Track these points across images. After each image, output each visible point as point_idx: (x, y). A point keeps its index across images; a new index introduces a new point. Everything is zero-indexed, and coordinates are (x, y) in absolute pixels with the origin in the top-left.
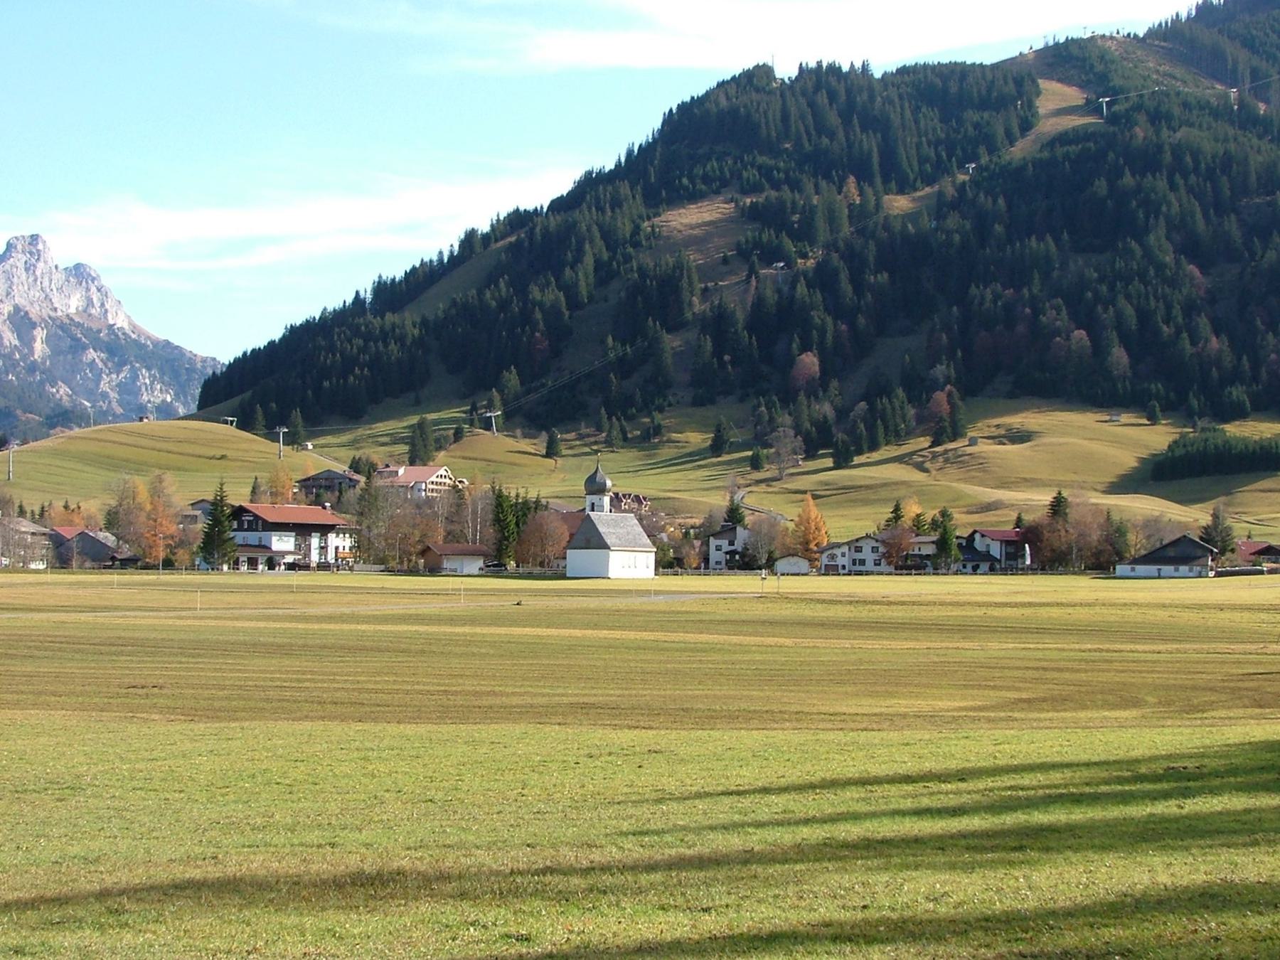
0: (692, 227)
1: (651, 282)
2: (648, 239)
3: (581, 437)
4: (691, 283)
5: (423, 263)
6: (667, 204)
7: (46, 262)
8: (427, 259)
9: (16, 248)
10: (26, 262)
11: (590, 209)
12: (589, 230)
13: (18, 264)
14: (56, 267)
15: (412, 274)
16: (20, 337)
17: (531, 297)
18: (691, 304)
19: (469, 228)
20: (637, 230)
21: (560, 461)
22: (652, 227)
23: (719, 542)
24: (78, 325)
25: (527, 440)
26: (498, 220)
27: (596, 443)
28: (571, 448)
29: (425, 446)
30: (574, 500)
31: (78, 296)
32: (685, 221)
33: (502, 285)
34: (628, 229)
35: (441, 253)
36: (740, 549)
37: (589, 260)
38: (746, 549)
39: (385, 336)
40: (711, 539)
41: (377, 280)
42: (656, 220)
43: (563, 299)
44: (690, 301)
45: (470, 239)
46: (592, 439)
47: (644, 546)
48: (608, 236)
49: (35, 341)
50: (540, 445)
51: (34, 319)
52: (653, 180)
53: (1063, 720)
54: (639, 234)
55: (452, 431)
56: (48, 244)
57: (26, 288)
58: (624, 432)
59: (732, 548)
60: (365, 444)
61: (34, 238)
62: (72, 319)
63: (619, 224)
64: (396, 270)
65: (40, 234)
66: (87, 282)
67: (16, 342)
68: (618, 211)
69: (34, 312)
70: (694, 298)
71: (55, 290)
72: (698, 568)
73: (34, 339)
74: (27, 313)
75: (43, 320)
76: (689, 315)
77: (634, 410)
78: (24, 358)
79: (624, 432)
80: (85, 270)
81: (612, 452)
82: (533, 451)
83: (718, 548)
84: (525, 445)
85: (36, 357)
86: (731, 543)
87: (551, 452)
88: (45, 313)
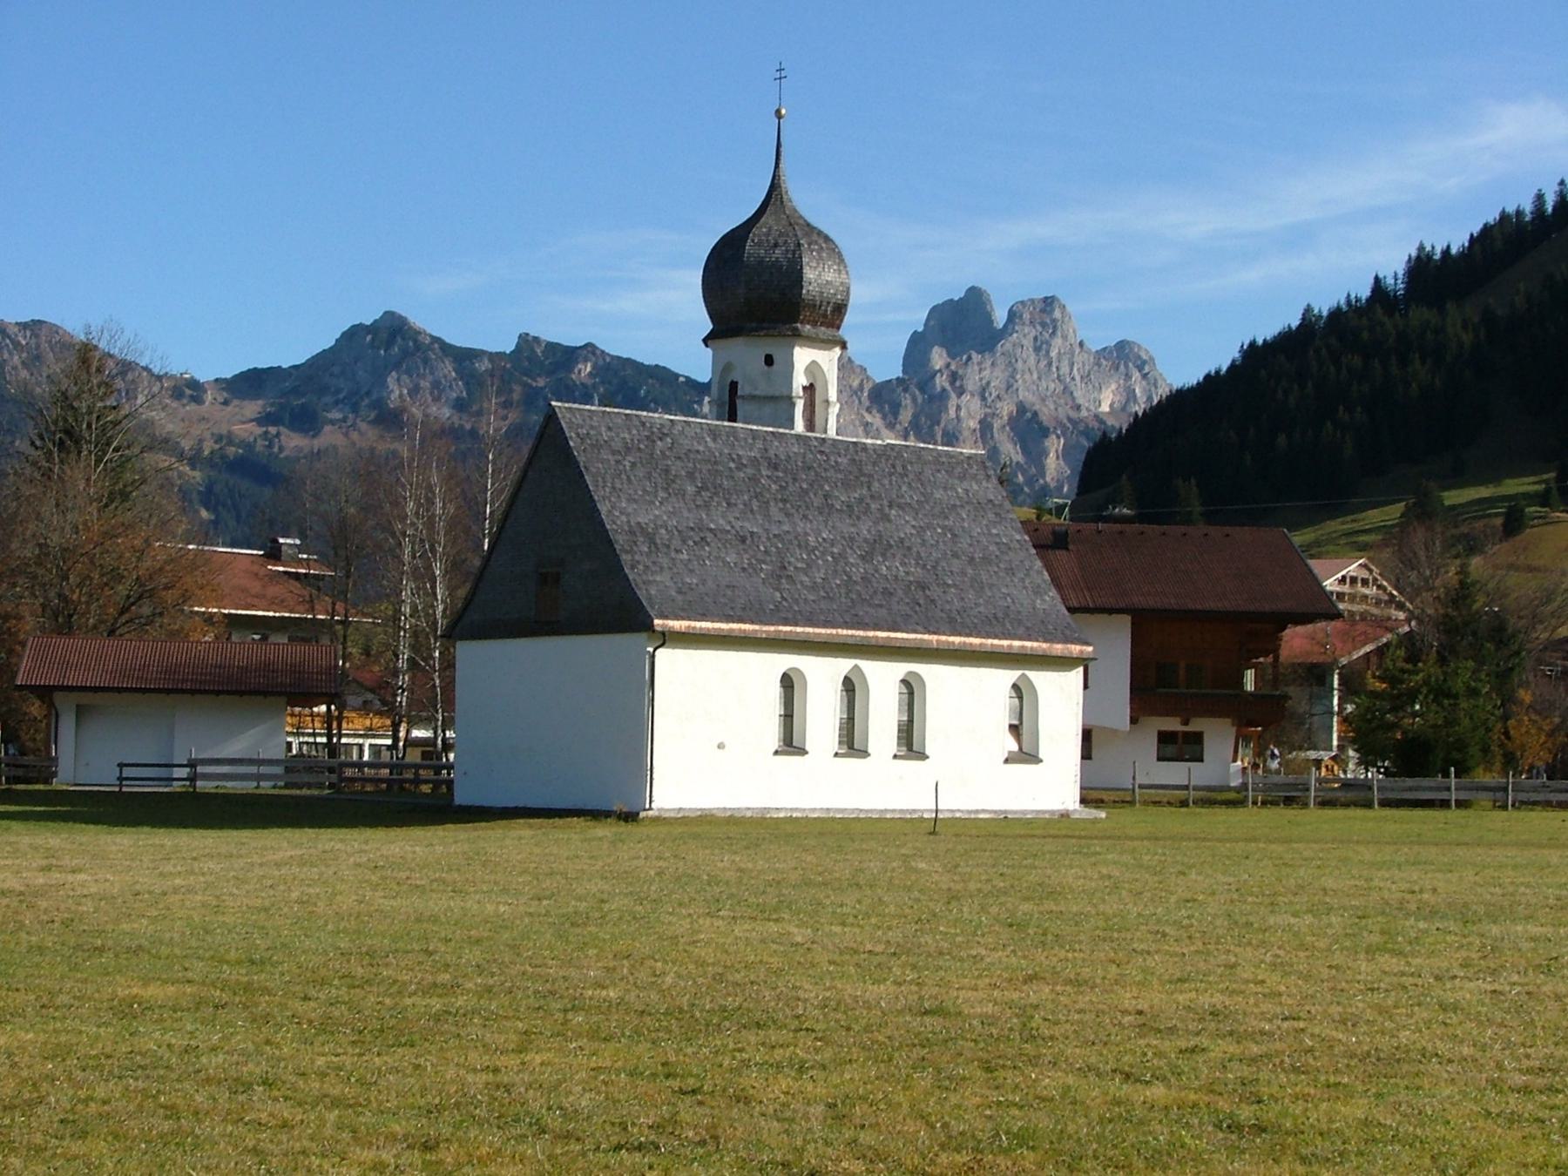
5: (1504, 217)
7: (1065, 338)
8: (1511, 209)
9: (1021, 316)
10: (1036, 339)
13: (1025, 342)
14: (1081, 344)
16: (1025, 451)
31: (1114, 386)
35: (1540, 198)
38: (1474, 584)
41: (1414, 254)
49: (1047, 455)
51: (1045, 423)
56: (1069, 309)
57: (1035, 376)
60: (1331, 548)
61: (1049, 302)
62: (1102, 422)
64: (1454, 236)
65: (1058, 295)
66: (1126, 366)
67: (1018, 457)
69: (1046, 413)
71: (1078, 378)
74: (1035, 414)
78: (1030, 481)
85: (1048, 479)
88: (1062, 414)
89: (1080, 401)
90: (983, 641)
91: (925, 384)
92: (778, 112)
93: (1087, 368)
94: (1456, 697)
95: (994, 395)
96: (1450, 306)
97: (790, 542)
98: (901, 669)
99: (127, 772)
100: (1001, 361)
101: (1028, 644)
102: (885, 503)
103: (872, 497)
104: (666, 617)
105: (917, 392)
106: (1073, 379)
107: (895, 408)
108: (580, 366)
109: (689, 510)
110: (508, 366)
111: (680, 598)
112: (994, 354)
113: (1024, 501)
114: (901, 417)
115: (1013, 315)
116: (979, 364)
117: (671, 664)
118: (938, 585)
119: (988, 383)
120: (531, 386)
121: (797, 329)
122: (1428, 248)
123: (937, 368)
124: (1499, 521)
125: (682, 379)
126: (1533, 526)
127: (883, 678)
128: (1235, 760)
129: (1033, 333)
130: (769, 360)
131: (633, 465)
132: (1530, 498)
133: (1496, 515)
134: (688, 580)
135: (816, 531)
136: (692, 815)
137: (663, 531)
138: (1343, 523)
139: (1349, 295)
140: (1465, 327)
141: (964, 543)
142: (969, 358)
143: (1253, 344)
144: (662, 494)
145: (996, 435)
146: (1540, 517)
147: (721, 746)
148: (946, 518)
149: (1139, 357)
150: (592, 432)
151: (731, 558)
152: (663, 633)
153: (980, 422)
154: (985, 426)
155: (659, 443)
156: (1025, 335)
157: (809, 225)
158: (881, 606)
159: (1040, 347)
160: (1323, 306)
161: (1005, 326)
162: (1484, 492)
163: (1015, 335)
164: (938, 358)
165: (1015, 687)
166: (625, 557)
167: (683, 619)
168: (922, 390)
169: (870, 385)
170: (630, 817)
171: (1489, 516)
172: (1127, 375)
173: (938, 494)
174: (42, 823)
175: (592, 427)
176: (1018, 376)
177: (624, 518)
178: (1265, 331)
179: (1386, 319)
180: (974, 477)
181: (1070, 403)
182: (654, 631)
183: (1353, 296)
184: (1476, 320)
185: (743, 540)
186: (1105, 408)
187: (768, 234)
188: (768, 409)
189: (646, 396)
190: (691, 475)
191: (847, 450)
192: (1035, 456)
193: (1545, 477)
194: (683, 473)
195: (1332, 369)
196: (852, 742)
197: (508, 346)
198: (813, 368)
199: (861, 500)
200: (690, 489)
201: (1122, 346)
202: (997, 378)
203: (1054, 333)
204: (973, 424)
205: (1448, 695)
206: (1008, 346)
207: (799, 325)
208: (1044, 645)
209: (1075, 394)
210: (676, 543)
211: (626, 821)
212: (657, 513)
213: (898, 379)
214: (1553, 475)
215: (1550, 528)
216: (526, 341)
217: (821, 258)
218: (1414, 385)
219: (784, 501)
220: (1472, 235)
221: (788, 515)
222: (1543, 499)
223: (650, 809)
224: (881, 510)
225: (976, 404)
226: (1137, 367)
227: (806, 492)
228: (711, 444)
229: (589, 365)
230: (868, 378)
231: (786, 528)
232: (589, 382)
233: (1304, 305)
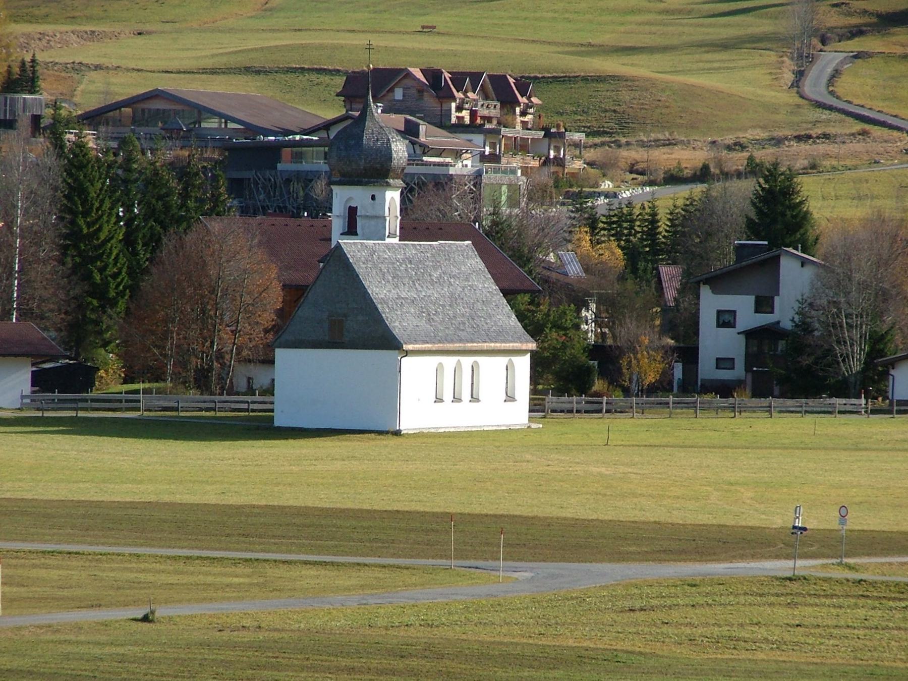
23: (727, 302)
30: (304, 78)
36: (787, 325)
38: (804, 327)
40: (705, 292)
47: (500, 335)
59: (764, 319)
72: (662, 387)
83: (725, 320)
86: (764, 304)
121: (387, 182)
130: (373, 198)
148: (469, 281)
152: (407, 352)
166: (383, 315)
187: (372, 133)
219: (419, 280)
231: (424, 294)
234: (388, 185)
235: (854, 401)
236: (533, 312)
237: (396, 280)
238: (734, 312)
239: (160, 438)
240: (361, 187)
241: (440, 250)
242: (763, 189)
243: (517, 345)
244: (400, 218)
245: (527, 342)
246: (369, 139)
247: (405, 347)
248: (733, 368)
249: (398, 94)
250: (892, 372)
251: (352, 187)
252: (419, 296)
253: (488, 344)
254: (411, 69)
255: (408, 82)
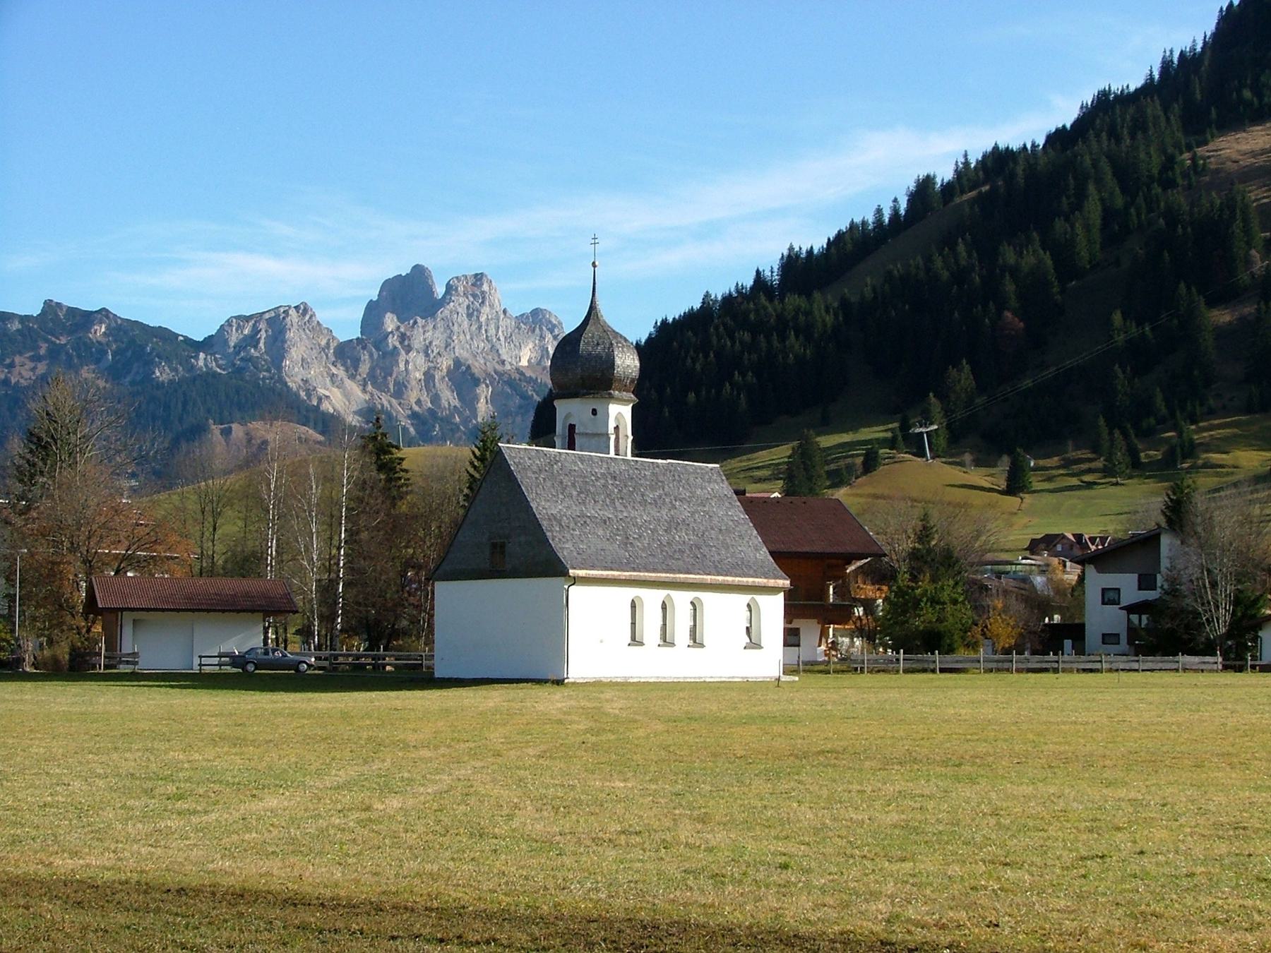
0: (1253, 154)
1: (1184, 228)
2: (1185, 175)
3: (1067, 464)
4: (1247, 231)
6: (1218, 129)
7: (491, 306)
8: (858, 220)
9: (457, 288)
10: (468, 307)
11: (1098, 136)
12: (1095, 164)
13: (460, 310)
14: (505, 312)
15: (838, 241)
16: (461, 397)
17: (1001, 261)
18: (1248, 262)
19: (922, 174)
20: (1170, 162)
21: (1028, 498)
22: (1193, 159)
24: (530, 380)
25: (984, 470)
26: (967, 163)
27: (1090, 471)
28: (1049, 479)
29: (810, 479)
31: (531, 345)
32: (1245, 147)
33: (961, 248)
34: (1156, 161)
35: (879, 211)
37: (1093, 209)
39: (782, 326)
41: (786, 253)
42: (1201, 151)
43: (1049, 262)
44: (1247, 255)
45: (923, 189)
46: (1085, 466)
48: (1125, 174)
49: (478, 401)
50: (996, 476)
51: (477, 375)
52: (1198, 96)
53: (1207, 472)
54: (1172, 169)
55: (862, 458)
57: (468, 337)
58: (1133, 453)
61: (479, 278)
62: (522, 374)
63: (1142, 156)
64: (815, 239)
65: (486, 272)
66: (541, 329)
67: (456, 403)
68: (1140, 135)
69: (478, 366)
70: (1253, 252)
71: (502, 339)
73: (476, 399)
74: (469, 367)
75: (489, 375)
76: (1244, 277)
77: (1152, 421)
78: (465, 421)
79: (1133, 453)
80: (544, 316)
81: (1117, 484)
82: (987, 485)
84: (978, 476)
85: (480, 420)
86: (1146, 582)
87: (1015, 486)
89: (504, 357)
90: (733, 578)
91: (380, 342)
92: (594, 263)
93: (509, 330)
94: (944, 603)
95: (435, 352)
96: (817, 295)
97: (629, 523)
98: (690, 595)
99: (204, 661)
100: (440, 324)
101: (757, 580)
102: (672, 497)
103: (666, 495)
104: (575, 568)
105: (374, 350)
106: (499, 339)
107: (356, 363)
108: (96, 327)
109: (576, 505)
110: (35, 326)
111: (578, 556)
112: (435, 319)
113: (460, 439)
114: (360, 370)
115: (450, 288)
116: (423, 327)
117: (577, 594)
118: (706, 546)
119: (431, 343)
120: (54, 343)
121: (610, 394)
122: (797, 249)
123: (390, 330)
124: (859, 460)
125: (181, 338)
126: (884, 465)
127: (682, 599)
128: (820, 646)
129: (467, 302)
130: (594, 412)
131: (544, 479)
132: (884, 443)
133: (858, 455)
134: (581, 546)
135: (641, 516)
136: (592, 681)
137: (565, 518)
138: (741, 461)
139: (737, 284)
140: (827, 310)
141: (715, 520)
142: (415, 322)
143: (664, 322)
144: (561, 496)
145: (437, 384)
146: (890, 458)
147: (601, 642)
148: (704, 506)
149: (550, 322)
150: (522, 461)
151: (600, 532)
152: (574, 578)
153: (424, 374)
154: (429, 377)
155: (555, 466)
156: (460, 303)
157: (614, 331)
158: (679, 559)
159: (472, 314)
160: (718, 292)
161: (444, 296)
162: (846, 438)
163: (452, 304)
164: (390, 322)
165: (749, 606)
166: (548, 534)
167: (583, 569)
168: (378, 349)
169: (333, 345)
170: (559, 682)
171: (852, 456)
172: (541, 336)
173: (699, 492)
174: (236, 691)
175: (521, 458)
176: (455, 337)
177: (544, 511)
178: (674, 311)
179: (767, 304)
180: (715, 481)
181: (496, 358)
182: (570, 576)
183: (740, 285)
184: (836, 304)
185: (605, 522)
186: (524, 363)
187: (592, 337)
188: (594, 441)
189: (151, 353)
190: (574, 485)
191: (649, 467)
192: (469, 400)
193: (890, 426)
194: (569, 484)
195: (729, 343)
196: (666, 640)
197: (35, 310)
198: (619, 417)
199: (660, 497)
200: (575, 493)
201: (536, 312)
202: (438, 338)
203: (483, 302)
204: (419, 375)
205: (938, 603)
206: (447, 313)
207: (612, 392)
208: (765, 580)
209: (500, 352)
210: (572, 525)
211: (558, 684)
212: (560, 507)
213: (358, 339)
214: (896, 425)
215: (897, 465)
216: (48, 304)
217: (623, 351)
218: (791, 356)
219: (622, 499)
220: (829, 239)
221: (625, 507)
222: (892, 444)
223: (567, 678)
224: (671, 502)
225: (421, 360)
226: (548, 329)
227: (632, 492)
228: (582, 467)
229: (103, 326)
230: (334, 338)
231: (625, 514)
232: (104, 340)
233: (704, 292)
234: (611, 397)
235: (1208, 659)
236: (913, 589)
237: (583, 496)
238: (1118, 590)
239: (233, 689)
240: (579, 399)
241: (667, 468)
242: (1171, 500)
243: (772, 583)
244: (631, 438)
245: (776, 577)
246: (588, 344)
247: (571, 572)
248: (1118, 644)
249: (1059, 548)
250: (1260, 634)
251: (570, 400)
252: (616, 517)
253: (713, 577)
254: (1066, 534)
255: (1065, 541)
